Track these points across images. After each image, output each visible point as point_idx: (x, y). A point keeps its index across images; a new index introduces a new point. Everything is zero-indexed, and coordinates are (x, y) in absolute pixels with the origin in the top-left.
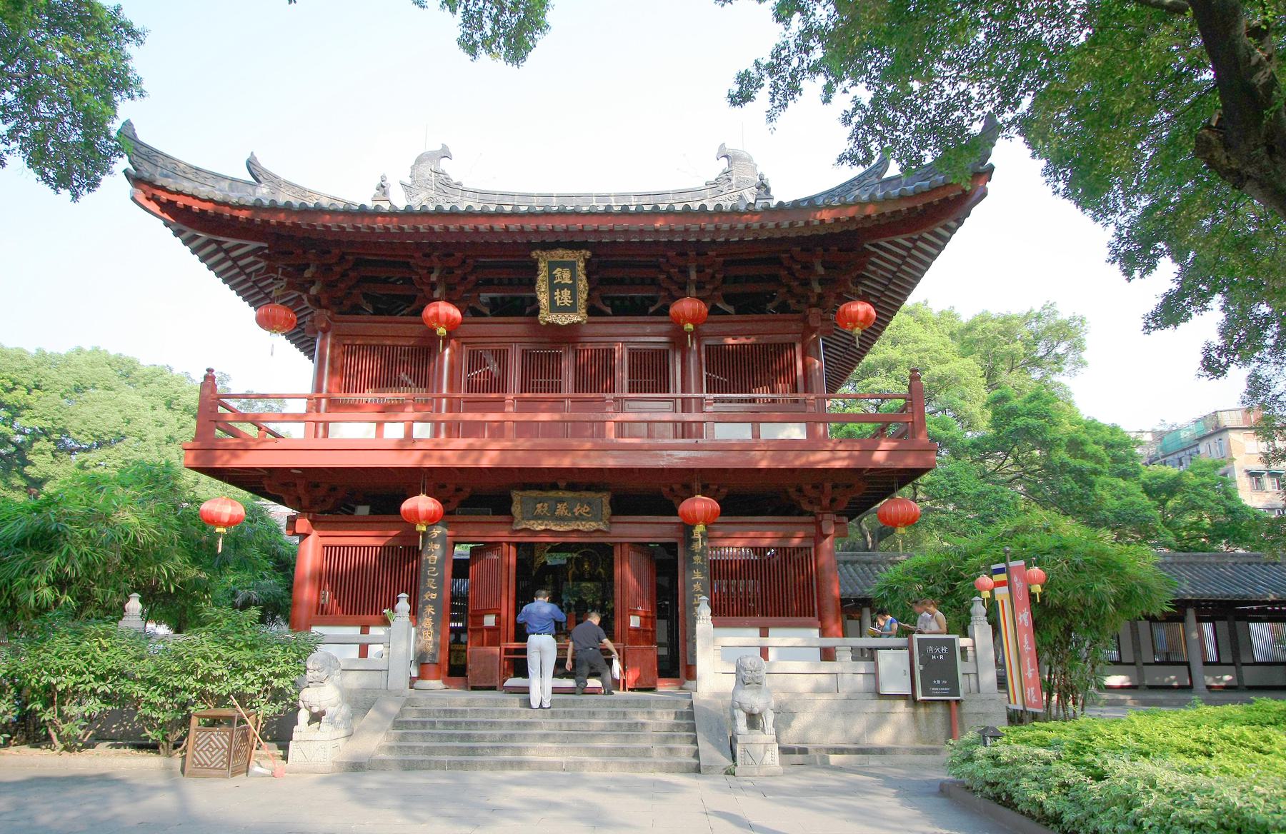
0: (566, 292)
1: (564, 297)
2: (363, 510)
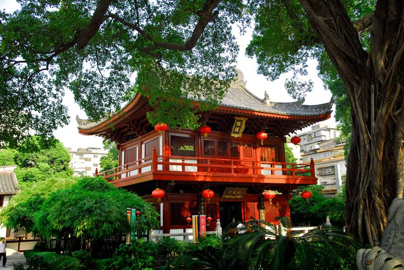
0: (238, 128)
1: (237, 130)
2: (181, 191)
